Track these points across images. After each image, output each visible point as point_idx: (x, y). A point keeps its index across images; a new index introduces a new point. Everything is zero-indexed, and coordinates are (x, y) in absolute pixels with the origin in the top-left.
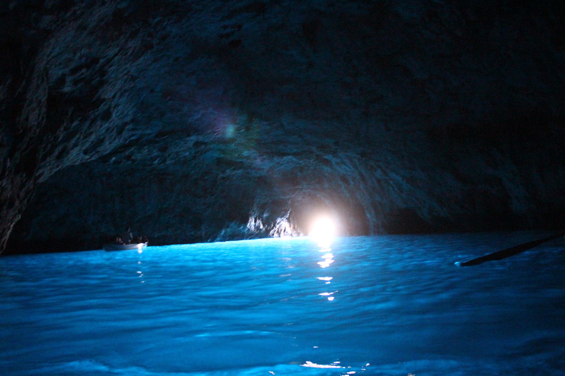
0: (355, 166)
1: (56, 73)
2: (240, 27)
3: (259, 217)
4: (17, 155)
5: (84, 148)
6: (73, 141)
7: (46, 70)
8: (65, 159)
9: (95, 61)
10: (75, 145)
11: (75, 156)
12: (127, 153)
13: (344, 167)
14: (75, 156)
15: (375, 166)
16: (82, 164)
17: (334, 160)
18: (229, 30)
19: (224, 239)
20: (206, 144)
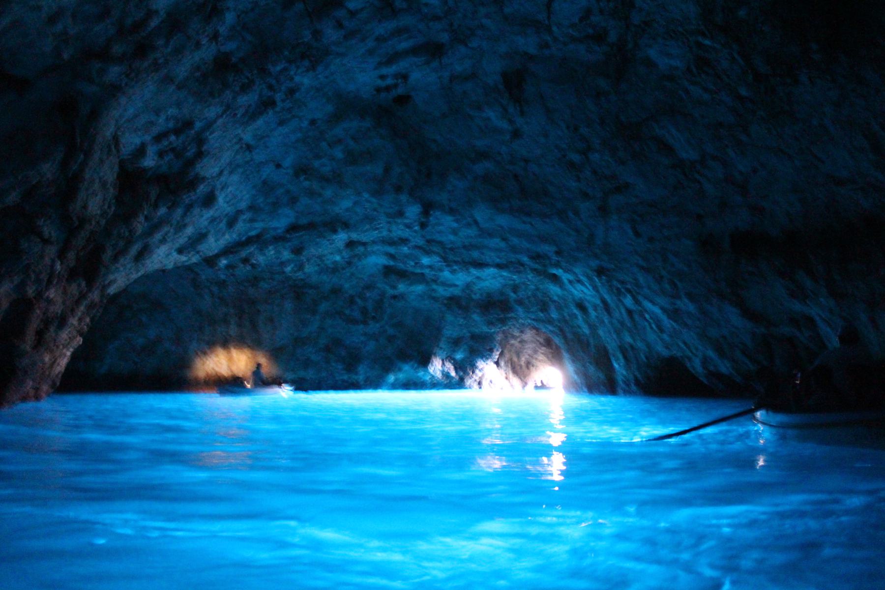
0: (595, 288)
1: (131, 141)
2: (405, 77)
3: (450, 358)
4: (71, 255)
5: (177, 245)
6: (158, 236)
7: (116, 139)
8: (148, 262)
9: (189, 124)
10: (163, 241)
11: (164, 256)
12: (244, 254)
13: (579, 287)
14: (164, 256)
15: (623, 290)
16: (177, 268)
17: (565, 277)
18: (389, 81)
19: (394, 387)
20: (364, 244)
